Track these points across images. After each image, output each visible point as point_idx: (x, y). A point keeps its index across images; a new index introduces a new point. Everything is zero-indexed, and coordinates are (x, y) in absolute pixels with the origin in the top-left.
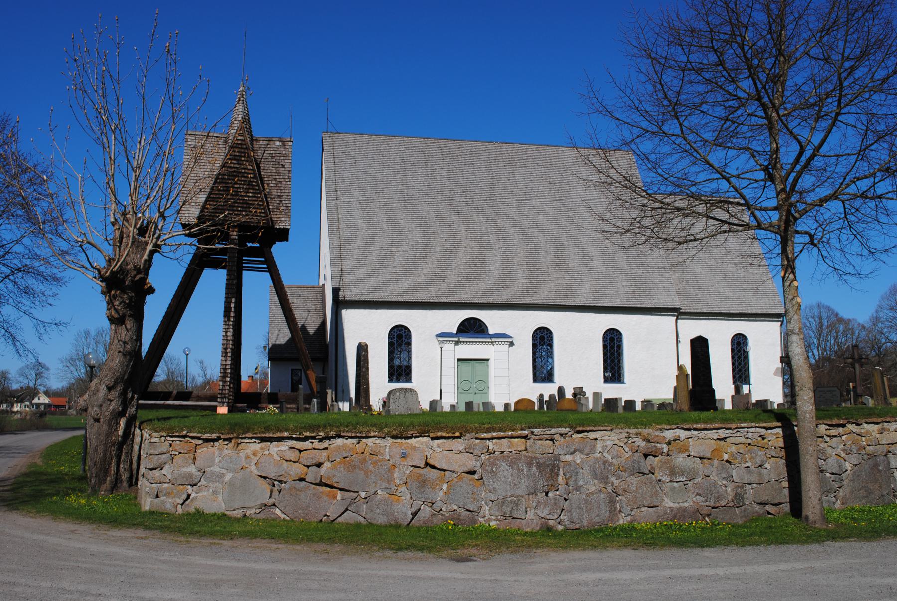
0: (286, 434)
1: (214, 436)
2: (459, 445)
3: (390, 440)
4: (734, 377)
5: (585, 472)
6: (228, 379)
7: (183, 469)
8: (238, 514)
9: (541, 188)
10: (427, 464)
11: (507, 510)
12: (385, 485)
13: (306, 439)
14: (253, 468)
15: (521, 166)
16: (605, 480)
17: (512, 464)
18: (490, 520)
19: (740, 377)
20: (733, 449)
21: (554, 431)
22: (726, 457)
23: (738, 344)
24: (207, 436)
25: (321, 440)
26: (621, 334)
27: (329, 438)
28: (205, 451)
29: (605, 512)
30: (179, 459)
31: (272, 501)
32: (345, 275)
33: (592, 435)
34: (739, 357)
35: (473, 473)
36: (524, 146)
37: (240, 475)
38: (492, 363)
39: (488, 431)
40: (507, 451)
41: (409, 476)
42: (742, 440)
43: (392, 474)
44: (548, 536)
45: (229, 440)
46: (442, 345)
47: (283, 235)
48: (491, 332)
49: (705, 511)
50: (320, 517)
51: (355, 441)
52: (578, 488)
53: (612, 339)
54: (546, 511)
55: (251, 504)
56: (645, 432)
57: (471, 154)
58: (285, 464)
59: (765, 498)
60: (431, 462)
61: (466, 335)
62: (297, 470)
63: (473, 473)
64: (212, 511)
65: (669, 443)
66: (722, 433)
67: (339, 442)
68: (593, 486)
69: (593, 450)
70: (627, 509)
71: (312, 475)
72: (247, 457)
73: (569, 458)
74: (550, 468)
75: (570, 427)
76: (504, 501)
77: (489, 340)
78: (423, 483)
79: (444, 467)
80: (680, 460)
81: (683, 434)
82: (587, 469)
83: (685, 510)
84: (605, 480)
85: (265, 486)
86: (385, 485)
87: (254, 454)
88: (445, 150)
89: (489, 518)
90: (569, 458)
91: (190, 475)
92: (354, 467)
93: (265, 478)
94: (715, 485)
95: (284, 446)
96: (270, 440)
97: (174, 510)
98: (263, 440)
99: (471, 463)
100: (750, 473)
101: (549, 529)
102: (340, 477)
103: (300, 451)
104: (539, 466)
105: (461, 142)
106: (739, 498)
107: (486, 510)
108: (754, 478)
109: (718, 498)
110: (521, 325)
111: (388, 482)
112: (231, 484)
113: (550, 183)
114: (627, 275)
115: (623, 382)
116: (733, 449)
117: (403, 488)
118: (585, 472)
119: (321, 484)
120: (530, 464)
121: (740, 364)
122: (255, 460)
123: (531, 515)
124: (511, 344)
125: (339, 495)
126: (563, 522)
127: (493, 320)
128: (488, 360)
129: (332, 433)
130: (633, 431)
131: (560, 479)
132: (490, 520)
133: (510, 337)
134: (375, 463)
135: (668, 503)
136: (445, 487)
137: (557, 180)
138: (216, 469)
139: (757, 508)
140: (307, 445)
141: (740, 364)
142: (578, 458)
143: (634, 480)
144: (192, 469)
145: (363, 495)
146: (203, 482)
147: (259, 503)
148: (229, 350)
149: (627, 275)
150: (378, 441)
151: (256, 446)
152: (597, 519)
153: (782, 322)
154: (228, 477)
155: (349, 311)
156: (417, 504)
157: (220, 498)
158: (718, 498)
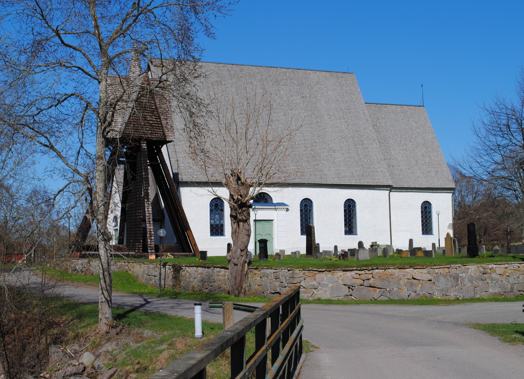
0: (355, 268)
1: (324, 270)
2: (425, 271)
3: (398, 270)
4: (423, 230)
5: (466, 280)
6: (153, 238)
7: (311, 283)
8: (337, 298)
9: (298, 101)
10: (413, 278)
11: (444, 293)
12: (397, 286)
13: (362, 270)
14: (341, 281)
15: (283, 85)
16: (472, 282)
17: (445, 277)
18: (438, 297)
19: (426, 230)
20: (510, 271)
21: (457, 265)
22: (507, 274)
23: (426, 208)
24: (320, 270)
25: (369, 270)
26: (355, 202)
27: (373, 269)
28: (319, 276)
29: (473, 293)
30: (308, 279)
31: (349, 294)
32: (181, 164)
33: (468, 267)
34: (426, 217)
35: (431, 280)
36: (284, 70)
37: (335, 284)
38: (275, 223)
39: (435, 266)
40: (442, 272)
41: (406, 282)
42: (512, 268)
43: (400, 282)
44: (457, 301)
45: (330, 271)
46: (256, 212)
47: (166, 142)
48: (274, 201)
49: (502, 293)
50: (371, 298)
51: (383, 270)
52: (465, 285)
53: (349, 206)
54: (456, 293)
55: (341, 295)
56: (483, 265)
57: (250, 75)
58: (354, 280)
59: (520, 289)
60: (414, 277)
61: (259, 204)
62: (360, 282)
63: (431, 280)
64: (325, 298)
65: (490, 269)
66: (506, 266)
67: (377, 271)
68: (469, 285)
69: (468, 272)
70: (479, 293)
71: (366, 283)
72: (338, 278)
73: (461, 275)
74: (456, 278)
75: (462, 264)
76: (443, 290)
77: (274, 207)
78: (412, 285)
79: (419, 279)
80: (494, 275)
81: (494, 266)
82: (467, 278)
83: (496, 293)
84: (472, 282)
85: (346, 288)
86: (397, 286)
87: (341, 276)
88: (232, 72)
89: (437, 295)
90: (461, 275)
91: (314, 285)
92: (384, 280)
93: (345, 285)
94: (504, 284)
95: (353, 273)
96: (347, 271)
97: (308, 299)
98: (344, 271)
99: (430, 277)
100: (515, 280)
101: (458, 299)
102: (378, 284)
103: (360, 275)
104: (453, 278)
105: (242, 67)
106: (512, 288)
107: (436, 293)
108: (516, 282)
109: (506, 289)
110: (293, 197)
111: (398, 285)
112: (332, 288)
113: (303, 97)
114: (357, 162)
115: (356, 234)
116: (510, 271)
117: (404, 287)
118: (466, 280)
119: (371, 287)
120: (451, 277)
121: (426, 221)
122: (341, 278)
123: (452, 294)
124: (288, 210)
125: (378, 290)
126: (461, 296)
127: (276, 194)
128: (272, 220)
129: (374, 268)
130: (480, 265)
131: (459, 282)
132: (438, 297)
133: (287, 205)
134: (392, 278)
135: (491, 290)
136: (420, 286)
137: (308, 95)
138: (325, 282)
139: (518, 292)
140: (363, 272)
141: (426, 221)
142: (464, 275)
143: (481, 282)
144: (314, 283)
145: (388, 290)
146: (320, 287)
147: (344, 294)
148: (151, 220)
149: (357, 162)
150: (393, 270)
151: (341, 273)
152: (471, 296)
153: (453, 194)
154: (330, 285)
155: (184, 188)
156: (409, 293)
157: (328, 293)
158: (506, 289)
